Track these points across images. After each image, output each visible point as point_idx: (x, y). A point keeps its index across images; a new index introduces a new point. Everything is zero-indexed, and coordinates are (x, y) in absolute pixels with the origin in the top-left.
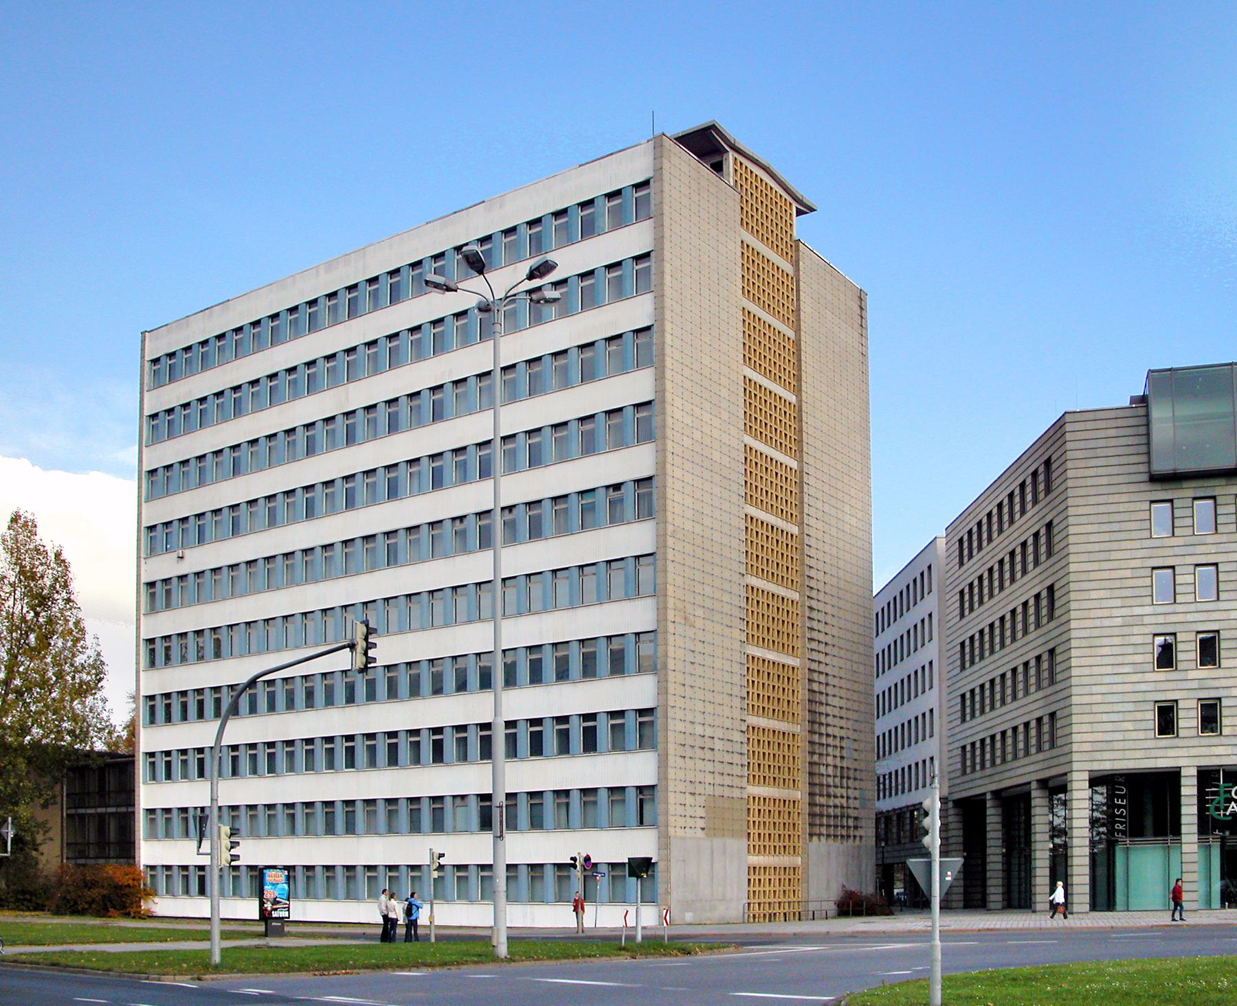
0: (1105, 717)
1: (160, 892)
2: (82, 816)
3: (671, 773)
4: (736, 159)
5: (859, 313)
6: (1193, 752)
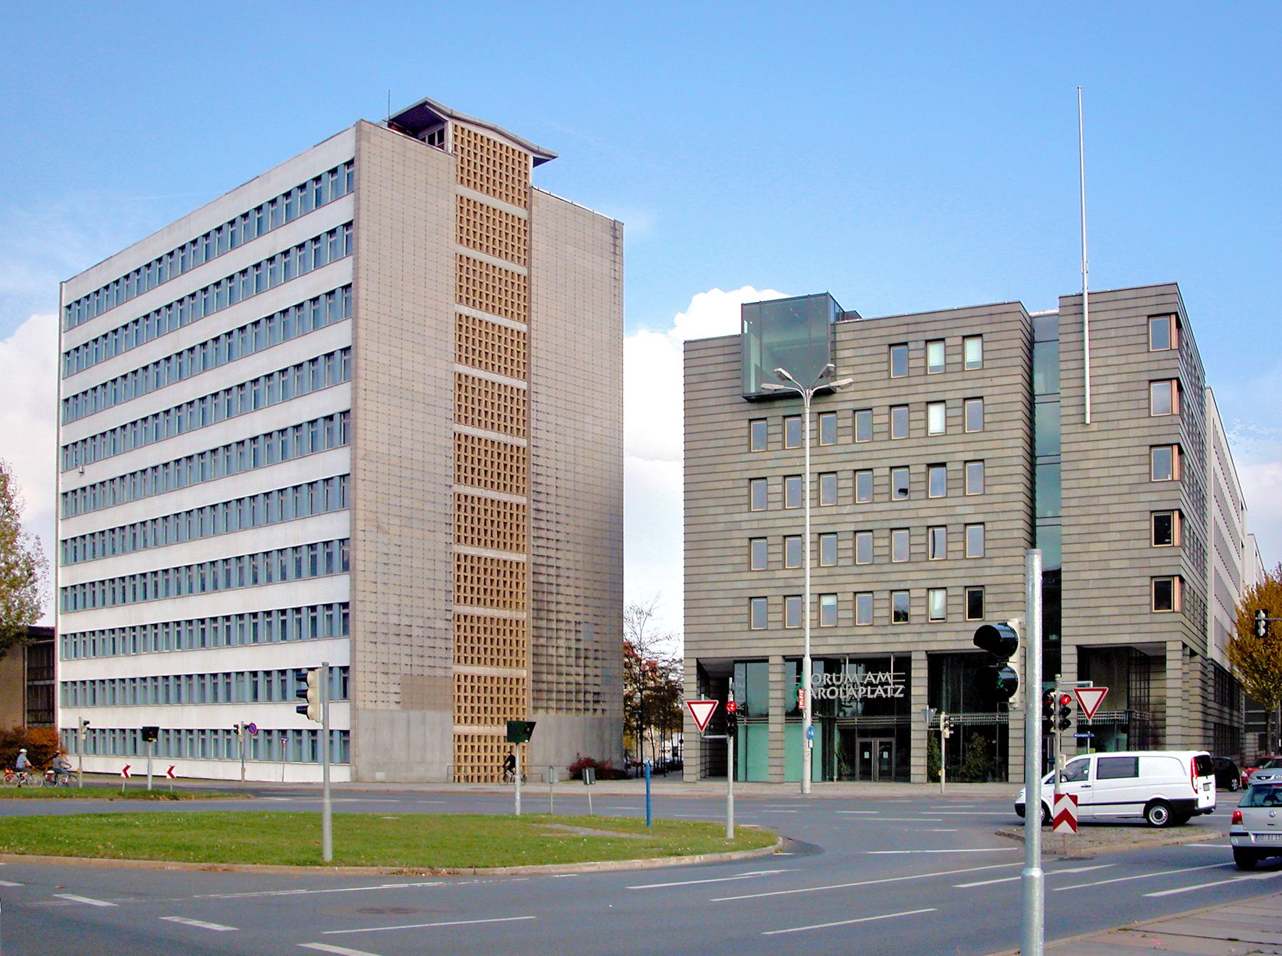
0: (710, 611)
1: (70, 750)
2: (37, 686)
3: (360, 656)
4: (456, 126)
6: (781, 643)
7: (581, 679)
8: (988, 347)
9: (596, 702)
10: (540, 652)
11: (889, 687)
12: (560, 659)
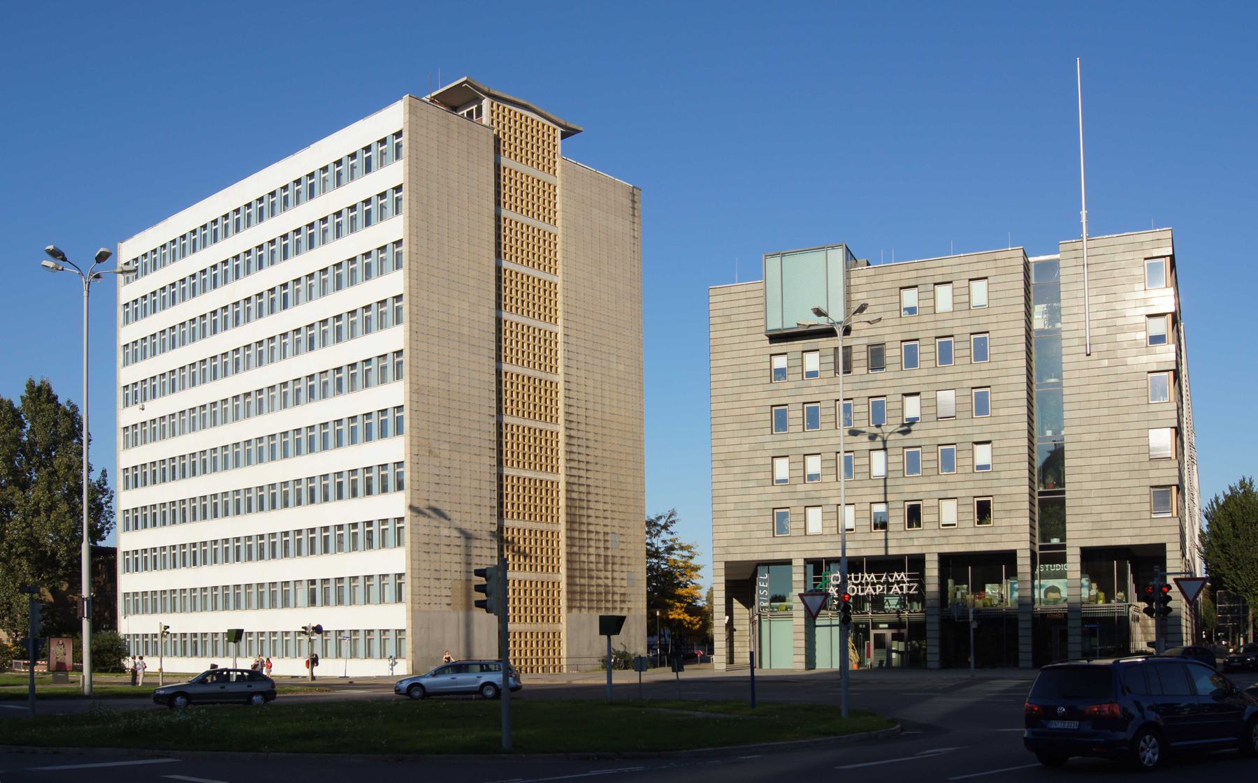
5: (631, 205)
7: (609, 582)
8: (992, 288)
9: (623, 601)
10: (573, 559)
11: (904, 585)
12: (591, 565)
